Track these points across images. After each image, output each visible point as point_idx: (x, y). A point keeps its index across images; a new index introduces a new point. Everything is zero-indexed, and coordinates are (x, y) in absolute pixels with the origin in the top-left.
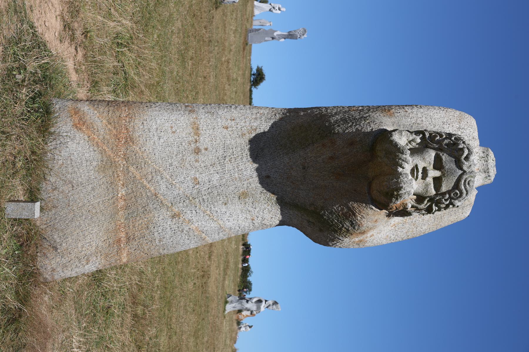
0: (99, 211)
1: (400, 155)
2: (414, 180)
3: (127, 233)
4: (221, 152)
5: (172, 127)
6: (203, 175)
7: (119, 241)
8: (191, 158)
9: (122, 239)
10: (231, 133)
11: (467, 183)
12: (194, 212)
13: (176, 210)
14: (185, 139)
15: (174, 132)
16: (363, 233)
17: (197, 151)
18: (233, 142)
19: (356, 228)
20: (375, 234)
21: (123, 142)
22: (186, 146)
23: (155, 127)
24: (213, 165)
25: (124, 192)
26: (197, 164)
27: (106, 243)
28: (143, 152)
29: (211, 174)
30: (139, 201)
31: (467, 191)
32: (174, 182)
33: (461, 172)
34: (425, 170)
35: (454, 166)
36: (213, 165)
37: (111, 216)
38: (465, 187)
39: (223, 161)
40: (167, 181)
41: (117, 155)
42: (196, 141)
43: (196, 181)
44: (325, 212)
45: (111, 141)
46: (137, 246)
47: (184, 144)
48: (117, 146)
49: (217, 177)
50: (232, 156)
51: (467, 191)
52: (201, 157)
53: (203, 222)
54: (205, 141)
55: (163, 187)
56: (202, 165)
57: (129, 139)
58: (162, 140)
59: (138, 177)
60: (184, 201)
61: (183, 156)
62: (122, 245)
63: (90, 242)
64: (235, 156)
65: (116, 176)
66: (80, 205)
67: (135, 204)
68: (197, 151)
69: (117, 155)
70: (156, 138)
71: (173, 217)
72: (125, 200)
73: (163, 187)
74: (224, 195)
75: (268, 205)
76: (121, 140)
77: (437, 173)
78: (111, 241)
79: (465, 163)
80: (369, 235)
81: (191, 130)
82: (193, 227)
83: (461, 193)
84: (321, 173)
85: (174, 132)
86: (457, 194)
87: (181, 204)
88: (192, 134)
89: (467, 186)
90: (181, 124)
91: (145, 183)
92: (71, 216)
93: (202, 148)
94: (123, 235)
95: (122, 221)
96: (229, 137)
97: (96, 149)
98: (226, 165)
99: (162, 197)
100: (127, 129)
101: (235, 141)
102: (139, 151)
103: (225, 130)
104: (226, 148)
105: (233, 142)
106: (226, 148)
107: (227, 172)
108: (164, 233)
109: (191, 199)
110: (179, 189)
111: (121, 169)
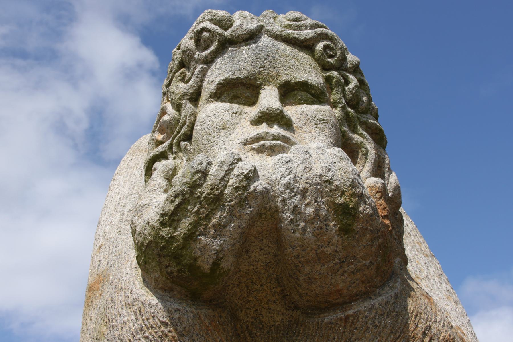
1: (210, 180)
38: (306, 29)
86: (326, 47)
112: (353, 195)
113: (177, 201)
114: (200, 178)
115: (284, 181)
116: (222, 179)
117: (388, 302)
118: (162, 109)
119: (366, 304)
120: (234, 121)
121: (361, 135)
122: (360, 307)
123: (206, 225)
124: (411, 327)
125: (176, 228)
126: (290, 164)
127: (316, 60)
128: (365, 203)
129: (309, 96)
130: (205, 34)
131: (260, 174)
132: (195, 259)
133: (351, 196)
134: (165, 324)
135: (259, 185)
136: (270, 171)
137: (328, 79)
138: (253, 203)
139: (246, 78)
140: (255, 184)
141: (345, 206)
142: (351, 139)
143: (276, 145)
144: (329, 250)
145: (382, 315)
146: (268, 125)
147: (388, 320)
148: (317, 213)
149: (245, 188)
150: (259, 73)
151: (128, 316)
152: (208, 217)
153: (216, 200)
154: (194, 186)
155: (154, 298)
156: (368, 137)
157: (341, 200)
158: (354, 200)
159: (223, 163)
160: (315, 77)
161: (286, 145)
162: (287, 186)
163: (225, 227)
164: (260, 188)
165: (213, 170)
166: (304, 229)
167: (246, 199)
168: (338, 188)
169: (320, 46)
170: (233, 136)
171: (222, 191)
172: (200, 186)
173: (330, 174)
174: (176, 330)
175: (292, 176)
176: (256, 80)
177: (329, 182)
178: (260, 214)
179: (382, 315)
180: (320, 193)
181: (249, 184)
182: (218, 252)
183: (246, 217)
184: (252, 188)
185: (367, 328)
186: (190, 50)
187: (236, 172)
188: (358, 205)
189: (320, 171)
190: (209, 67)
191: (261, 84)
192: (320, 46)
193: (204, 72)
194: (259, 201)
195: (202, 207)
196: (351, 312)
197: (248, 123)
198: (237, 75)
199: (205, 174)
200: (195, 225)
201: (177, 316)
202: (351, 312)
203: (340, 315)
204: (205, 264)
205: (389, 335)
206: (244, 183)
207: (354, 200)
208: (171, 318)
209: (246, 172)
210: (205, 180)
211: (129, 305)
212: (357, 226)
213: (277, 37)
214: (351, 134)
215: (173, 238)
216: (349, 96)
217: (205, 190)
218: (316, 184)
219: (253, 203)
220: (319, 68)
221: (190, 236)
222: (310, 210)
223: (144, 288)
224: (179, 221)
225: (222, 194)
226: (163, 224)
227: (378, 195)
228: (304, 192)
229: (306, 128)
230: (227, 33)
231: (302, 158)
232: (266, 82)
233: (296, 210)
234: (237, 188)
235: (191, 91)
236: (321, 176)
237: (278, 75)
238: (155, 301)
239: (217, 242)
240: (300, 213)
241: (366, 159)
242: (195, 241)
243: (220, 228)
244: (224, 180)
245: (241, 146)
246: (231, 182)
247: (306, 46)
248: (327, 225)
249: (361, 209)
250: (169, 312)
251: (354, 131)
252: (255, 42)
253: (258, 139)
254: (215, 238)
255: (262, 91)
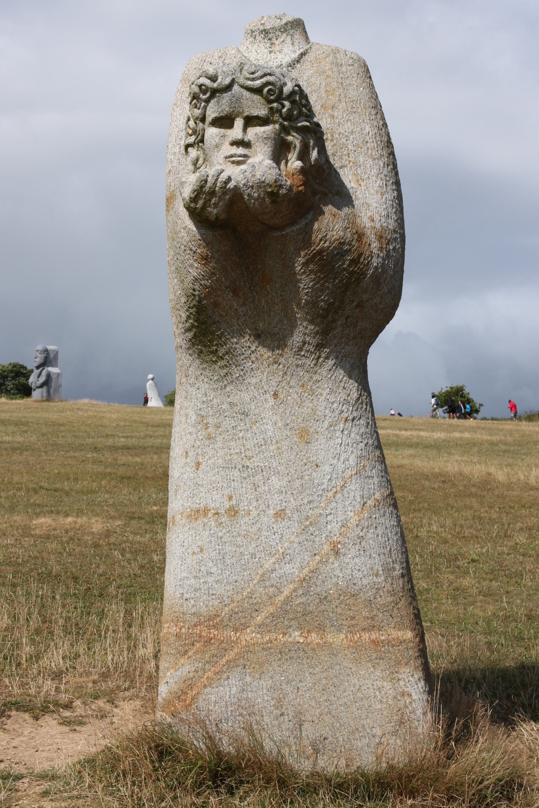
0: (325, 675)
1: (209, 185)
2: (250, 161)
3: (363, 630)
4: (236, 473)
5: (194, 553)
6: (270, 503)
7: (375, 643)
8: (243, 522)
9: (373, 637)
10: (207, 457)
11: (252, 76)
12: (329, 518)
13: (326, 548)
14: (212, 532)
15: (202, 550)
16: (360, 236)
17: (233, 512)
18: (221, 453)
19: (346, 248)
20: (369, 214)
21: (216, 633)
22: (224, 531)
23: (193, 580)
24: (256, 487)
25: (296, 633)
26: (254, 513)
27: (378, 663)
28: (233, 601)
29: (269, 489)
30: (311, 608)
31: (265, 75)
32: (281, 551)
33: (236, 87)
34: (237, 143)
35: (227, 96)
36: (256, 487)
37: (334, 654)
38: (258, 79)
39: (249, 470)
40: (278, 561)
41: (236, 642)
42: (217, 514)
43: (280, 515)
44: (323, 300)
45: (213, 652)
46: (385, 613)
47: (220, 534)
48: (222, 642)
49: (275, 482)
50: (243, 455)
51: (265, 75)
52: (243, 506)
53: (347, 503)
54: (217, 500)
55: (288, 568)
56: (255, 504)
57: (211, 623)
58: (214, 570)
59: (271, 609)
60: (312, 534)
61: (239, 535)
62: (383, 638)
63: (374, 689)
64: (243, 451)
65: (269, 645)
66: (313, 704)
67: (306, 612)
68: (233, 512)
69: (236, 642)
70: (210, 579)
71: (337, 553)
72: (309, 632)
73: (288, 568)
74: (303, 469)
75: (321, 394)
76: (212, 635)
77: (239, 123)
78: (374, 655)
79: (219, 80)
80: (368, 225)
81: (199, 522)
82: (353, 522)
83: (268, 83)
84: (264, 307)
85: (202, 550)
86: (270, 90)
87: (317, 539)
88: (206, 520)
89: (256, 75)
90: (190, 538)
91: (281, 598)
92: (328, 719)
93: (227, 505)
94: (366, 636)
95: (342, 636)
96: (213, 460)
97: (225, 676)
98: (256, 464)
99: (304, 571)
100: (195, 625)
101: (219, 451)
102: (230, 607)
103: (202, 467)
104: (229, 466)
105: (221, 453)
106: (229, 466)
107: (267, 464)
108: (364, 568)
109: (308, 523)
110: (292, 542)
111: (259, 636)
112: (276, 186)
113: (195, 193)
114: (204, 183)
115: (243, 183)
116: (214, 184)
117: (301, 228)
118: (145, 398)
119: (291, 229)
120: (221, 142)
121: (293, 136)
122: (288, 230)
123: (210, 204)
124: (313, 239)
125: (197, 204)
126: (245, 174)
127: (264, 98)
128: (283, 188)
129: (260, 122)
130: (203, 87)
131: (232, 177)
132: (208, 217)
133: (275, 187)
134: (200, 240)
135: (231, 185)
136: (237, 175)
137: (271, 109)
138: (229, 193)
139: (226, 115)
140: (229, 185)
141: (272, 192)
142: (286, 140)
143: (240, 161)
144: (267, 210)
145: (298, 234)
146: (237, 146)
147: (301, 236)
148: (259, 195)
149: (225, 187)
150: (233, 111)
151: (183, 233)
152: (210, 200)
153: (212, 193)
154: (202, 187)
155: (194, 227)
156: (297, 136)
157: (270, 190)
158: (276, 188)
159: (213, 176)
160: (262, 111)
161: (245, 159)
162: (244, 185)
163: (218, 204)
164: (232, 187)
165: (210, 179)
166: (254, 203)
167: (226, 192)
168: (268, 184)
169: (266, 90)
170: (221, 151)
171: (215, 189)
172: (205, 187)
173: (264, 178)
174: (205, 242)
175: (246, 180)
176: (231, 116)
177: (264, 182)
178: (234, 197)
179: (298, 234)
180: (260, 187)
181: (226, 186)
182: (216, 214)
183: (227, 200)
184: (228, 187)
185: (291, 240)
186: (197, 93)
187: (220, 180)
188: (278, 191)
189: (259, 177)
190: (208, 105)
191: (235, 117)
192: (266, 90)
193: (205, 108)
194: (232, 192)
195: (207, 196)
196: (284, 233)
197: (229, 146)
198: (221, 114)
199: (206, 181)
200: (205, 204)
201: (204, 237)
202: (284, 233)
203: (279, 234)
204: (213, 218)
205: (301, 243)
206: (224, 185)
207: (276, 188)
208: (202, 238)
209: (224, 180)
210: (206, 184)
211: (184, 228)
212: (279, 200)
213: (242, 87)
214: (286, 137)
215: (196, 208)
216: (284, 116)
217: (207, 188)
218: (258, 183)
219: (229, 193)
220: (265, 103)
221: (204, 208)
222: (256, 195)
223: (190, 220)
224: (197, 201)
225: (215, 190)
226: (191, 202)
227: (298, 173)
228: (252, 187)
229: (257, 144)
230: (215, 85)
231: (251, 169)
232: (237, 116)
233: (249, 195)
234: (221, 188)
235: (200, 117)
236: (259, 179)
237: (243, 112)
238: (195, 229)
239: (215, 210)
240: (251, 196)
241: (295, 150)
242: (206, 209)
243: (216, 205)
244: (215, 184)
245: (224, 159)
246: (218, 184)
247: (258, 91)
248: (265, 201)
249: (280, 192)
250: (201, 234)
251: (289, 134)
252: (230, 90)
253: (232, 156)
254: (214, 209)
255: (235, 122)
